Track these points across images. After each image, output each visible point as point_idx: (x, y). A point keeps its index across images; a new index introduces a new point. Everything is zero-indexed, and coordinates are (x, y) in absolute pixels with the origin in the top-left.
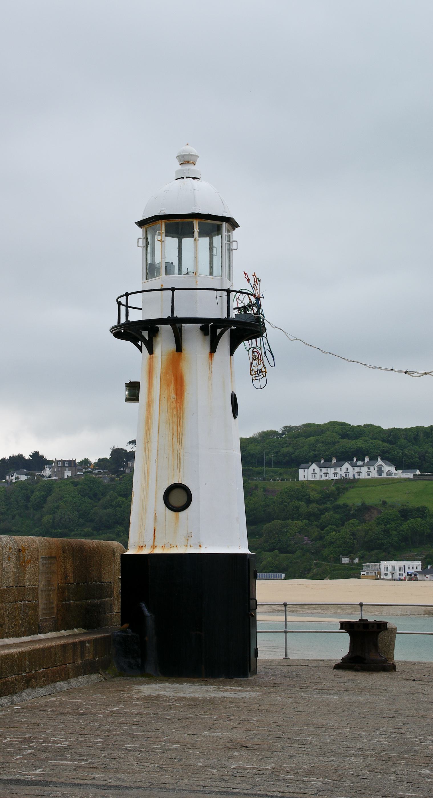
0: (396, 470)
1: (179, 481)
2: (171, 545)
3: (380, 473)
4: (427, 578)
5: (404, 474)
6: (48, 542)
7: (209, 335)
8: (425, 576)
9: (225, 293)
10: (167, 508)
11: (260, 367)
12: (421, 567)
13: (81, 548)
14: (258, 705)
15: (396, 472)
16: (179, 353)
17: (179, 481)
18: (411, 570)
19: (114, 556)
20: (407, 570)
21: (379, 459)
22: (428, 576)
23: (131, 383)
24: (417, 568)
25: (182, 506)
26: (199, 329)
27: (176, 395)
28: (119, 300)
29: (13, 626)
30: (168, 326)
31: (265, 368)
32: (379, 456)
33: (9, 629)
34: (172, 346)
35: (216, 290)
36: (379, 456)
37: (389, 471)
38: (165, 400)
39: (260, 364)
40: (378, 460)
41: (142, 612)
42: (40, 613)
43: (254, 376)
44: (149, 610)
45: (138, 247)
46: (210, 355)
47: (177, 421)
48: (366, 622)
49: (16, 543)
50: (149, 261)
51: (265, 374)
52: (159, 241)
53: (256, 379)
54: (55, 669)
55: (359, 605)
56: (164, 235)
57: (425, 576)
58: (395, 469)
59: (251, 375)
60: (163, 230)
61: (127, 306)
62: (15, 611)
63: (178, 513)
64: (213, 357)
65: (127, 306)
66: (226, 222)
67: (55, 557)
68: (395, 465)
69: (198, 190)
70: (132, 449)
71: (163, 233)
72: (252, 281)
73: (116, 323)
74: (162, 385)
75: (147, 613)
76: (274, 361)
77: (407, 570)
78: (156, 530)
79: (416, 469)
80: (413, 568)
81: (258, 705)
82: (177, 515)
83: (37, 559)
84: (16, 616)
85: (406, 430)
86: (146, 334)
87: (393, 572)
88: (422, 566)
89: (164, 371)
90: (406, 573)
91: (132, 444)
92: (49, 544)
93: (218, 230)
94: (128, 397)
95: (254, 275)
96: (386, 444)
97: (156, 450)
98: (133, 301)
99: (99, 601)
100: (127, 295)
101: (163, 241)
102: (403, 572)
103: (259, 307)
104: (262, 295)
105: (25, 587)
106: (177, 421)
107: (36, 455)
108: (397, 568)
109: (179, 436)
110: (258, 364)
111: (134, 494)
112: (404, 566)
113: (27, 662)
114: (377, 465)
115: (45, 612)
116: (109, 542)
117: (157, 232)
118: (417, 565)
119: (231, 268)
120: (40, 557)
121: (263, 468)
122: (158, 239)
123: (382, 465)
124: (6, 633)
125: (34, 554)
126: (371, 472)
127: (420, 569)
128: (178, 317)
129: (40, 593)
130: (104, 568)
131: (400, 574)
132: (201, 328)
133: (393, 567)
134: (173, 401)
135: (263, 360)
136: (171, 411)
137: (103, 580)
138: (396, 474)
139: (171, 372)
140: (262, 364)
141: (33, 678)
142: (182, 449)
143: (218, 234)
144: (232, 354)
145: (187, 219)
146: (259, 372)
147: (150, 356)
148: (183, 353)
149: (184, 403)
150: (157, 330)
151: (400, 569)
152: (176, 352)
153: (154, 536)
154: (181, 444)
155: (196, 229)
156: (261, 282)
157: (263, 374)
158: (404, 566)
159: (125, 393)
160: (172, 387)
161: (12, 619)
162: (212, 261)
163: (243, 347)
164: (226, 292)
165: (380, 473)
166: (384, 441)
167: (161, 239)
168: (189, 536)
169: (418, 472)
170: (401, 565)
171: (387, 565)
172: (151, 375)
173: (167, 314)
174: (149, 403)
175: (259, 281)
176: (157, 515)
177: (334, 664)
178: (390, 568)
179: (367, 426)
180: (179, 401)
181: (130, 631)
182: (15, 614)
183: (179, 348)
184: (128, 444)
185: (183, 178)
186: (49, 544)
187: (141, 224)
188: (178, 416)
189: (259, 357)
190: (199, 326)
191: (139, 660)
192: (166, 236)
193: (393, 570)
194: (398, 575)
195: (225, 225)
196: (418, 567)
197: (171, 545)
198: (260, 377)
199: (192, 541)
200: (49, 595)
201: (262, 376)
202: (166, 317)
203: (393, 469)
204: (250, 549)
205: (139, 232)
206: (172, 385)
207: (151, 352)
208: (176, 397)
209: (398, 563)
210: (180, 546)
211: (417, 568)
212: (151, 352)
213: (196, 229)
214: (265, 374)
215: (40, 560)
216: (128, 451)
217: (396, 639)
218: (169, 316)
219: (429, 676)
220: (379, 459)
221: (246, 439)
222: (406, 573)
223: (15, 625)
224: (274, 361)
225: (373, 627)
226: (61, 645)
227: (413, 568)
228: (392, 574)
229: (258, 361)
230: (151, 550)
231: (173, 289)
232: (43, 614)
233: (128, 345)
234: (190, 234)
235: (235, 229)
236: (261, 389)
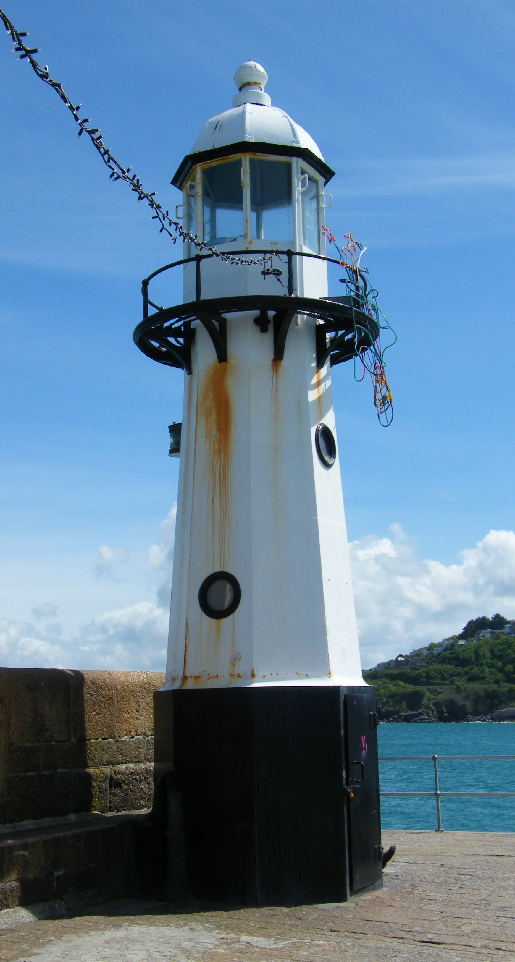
1: (222, 569)
2: (209, 674)
9: (285, 257)
14: (496, 918)
17: (222, 569)
27: (219, 430)
45: (177, 207)
47: (220, 472)
63: (220, 620)
64: (278, 370)
69: (251, 113)
74: (199, 419)
78: (188, 650)
81: (496, 918)
106: (220, 472)
107: (497, 617)
109: (222, 496)
128: (205, 299)
134: (213, 441)
139: (211, 395)
145: (231, 156)
148: (228, 365)
149: (230, 441)
152: (218, 364)
160: (214, 417)
176: (189, 625)
179: (148, 356)
197: (209, 674)
201: (388, 405)
202: (179, 301)
208: (218, 433)
219: (431, 900)
236: (388, 425)
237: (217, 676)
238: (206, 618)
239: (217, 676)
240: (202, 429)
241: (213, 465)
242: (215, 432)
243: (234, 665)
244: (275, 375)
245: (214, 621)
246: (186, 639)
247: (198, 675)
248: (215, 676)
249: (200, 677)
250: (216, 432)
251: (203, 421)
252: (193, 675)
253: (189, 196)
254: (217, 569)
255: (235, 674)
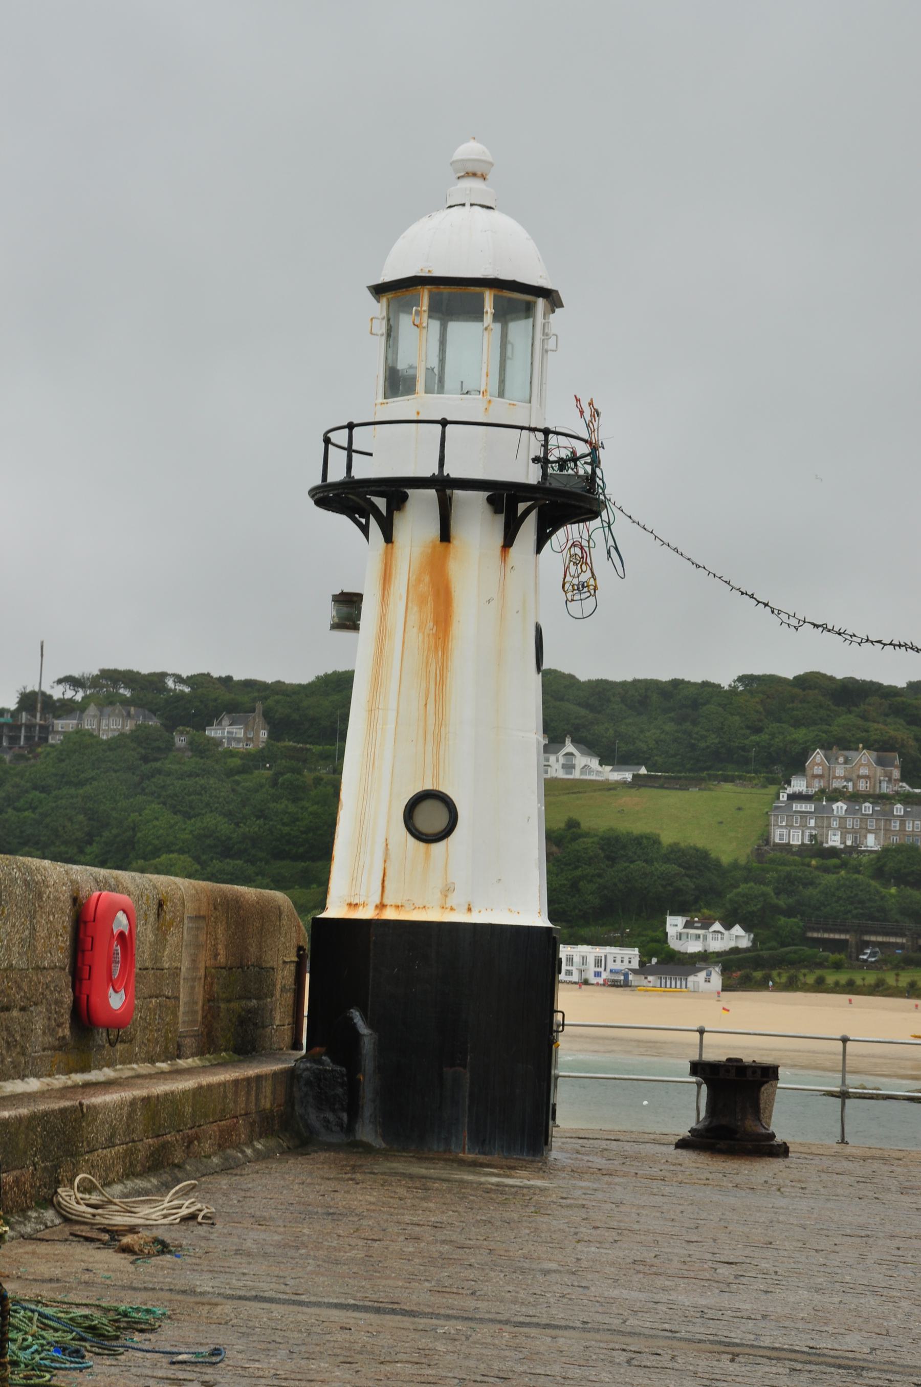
0: (601, 764)
3: (568, 767)
4: (650, 982)
5: (616, 774)
6: (194, 887)
7: (502, 513)
8: (646, 978)
9: (541, 436)
10: (409, 836)
11: (585, 577)
12: (638, 959)
13: (237, 902)
15: (599, 768)
16: (445, 544)
18: (618, 966)
19: (280, 920)
20: (611, 965)
21: (568, 741)
22: (650, 978)
23: (343, 594)
24: (630, 962)
25: (435, 835)
26: (486, 501)
27: (436, 622)
28: (329, 435)
29: (146, 1041)
30: (432, 493)
31: (595, 580)
32: (568, 736)
33: (140, 1048)
34: (434, 530)
35: (522, 428)
36: (568, 736)
37: (585, 766)
38: (413, 632)
39: (584, 570)
40: (567, 742)
41: (353, 1027)
42: (180, 1021)
43: (569, 595)
44: (370, 1024)
45: (372, 319)
46: (502, 551)
48: (739, 1064)
49: (155, 887)
50: (390, 361)
51: (595, 590)
52: (417, 326)
53: (573, 600)
54: (224, 1125)
55: (697, 1031)
56: (425, 315)
57: (646, 978)
58: (597, 762)
59: (564, 590)
60: (425, 307)
61: (350, 450)
62: (150, 1013)
65: (350, 450)
66: (544, 297)
67: (204, 917)
68: (598, 756)
70: (63, 694)
71: (425, 311)
72: (587, 415)
73: (318, 481)
74: (410, 605)
75: (363, 1029)
76: (623, 566)
77: (611, 965)
78: (387, 874)
79: (639, 764)
80: (622, 961)
82: (427, 849)
83: (182, 920)
84: (150, 1024)
85: (624, 684)
86: (381, 503)
87: (583, 968)
88: (640, 957)
89: (414, 577)
90: (608, 970)
91: (64, 684)
92: (197, 893)
93: (528, 310)
94: (336, 620)
95: (591, 404)
96: (583, 712)
97: (394, 726)
98: (361, 438)
99: (254, 1002)
100: (351, 426)
101: (424, 328)
102: (602, 969)
103: (595, 462)
104: (602, 443)
105: (163, 970)
108: (591, 961)
110: (579, 571)
111: (342, 806)
112: (606, 957)
113: (190, 1110)
114: (565, 752)
115: (187, 1019)
116: (272, 892)
117: (414, 308)
118: (630, 956)
119: (544, 386)
120: (185, 918)
121: (333, 747)
122: (416, 323)
123: (572, 754)
124: (136, 1054)
125: (178, 911)
126: (549, 766)
127: (635, 965)
129: (182, 982)
130: (265, 941)
131: (595, 972)
132: (490, 500)
133: (583, 958)
134: (429, 635)
135: (591, 563)
136: (425, 653)
137: (264, 965)
138: (600, 772)
139: (427, 579)
140: (589, 571)
141: (196, 1139)
142: (443, 726)
143: (527, 317)
144: (539, 550)
146: (582, 586)
147: (387, 546)
148: (451, 545)
150: (405, 497)
151: (598, 962)
153: (383, 887)
154: (440, 716)
155: (489, 307)
156: (602, 416)
157: (589, 591)
158: (606, 957)
159: (328, 612)
161: (146, 1028)
162: (504, 370)
163: (561, 537)
164: (542, 433)
165: (568, 767)
166: (579, 704)
167: (421, 323)
168: (447, 891)
169: (643, 771)
170: (599, 955)
171: (571, 954)
172: (387, 586)
173: (429, 469)
174: (382, 635)
175: (598, 416)
176: (389, 847)
177: (675, 1140)
178: (577, 959)
180: (441, 635)
181: (329, 1060)
182: (150, 1019)
183: (445, 536)
184: (55, 684)
185: (464, 205)
186: (197, 893)
187: (379, 290)
188: (437, 662)
189: (583, 558)
190: (487, 494)
191: (345, 1116)
192: (430, 317)
193: (583, 964)
194: (593, 974)
195: (541, 303)
196: (632, 960)
198: (584, 596)
199: (453, 900)
200: (193, 987)
201: (588, 594)
202: (428, 474)
203: (594, 763)
204: (551, 919)
205: (378, 308)
206: (429, 604)
207: (388, 538)
208: (435, 627)
209: (594, 950)
210: (477, 911)
211: (630, 962)
212: (388, 538)
213: (489, 307)
214: (595, 590)
215: (186, 921)
216: (55, 698)
217: (777, 1098)
218: (434, 474)
220: (568, 741)
221: (300, 685)
222: (608, 970)
223: (148, 1040)
224: (623, 566)
225: (754, 1072)
226: (233, 1081)
227: (622, 961)
228: (581, 971)
229: (581, 566)
230: (377, 912)
231: (444, 423)
232: (184, 1022)
233: (342, 523)
234: (476, 314)
235: (553, 311)
237: (425, 907)
238: (411, 840)
239: (425, 907)
240: (414, 618)
241: (427, 663)
242: (430, 624)
243: (446, 896)
244: (503, 564)
245: (422, 845)
246: (385, 861)
247: (400, 904)
248: (422, 906)
249: (402, 906)
250: (431, 624)
251: (416, 609)
252: (393, 904)
253: (382, 306)
254: (428, 786)
255: (447, 906)
